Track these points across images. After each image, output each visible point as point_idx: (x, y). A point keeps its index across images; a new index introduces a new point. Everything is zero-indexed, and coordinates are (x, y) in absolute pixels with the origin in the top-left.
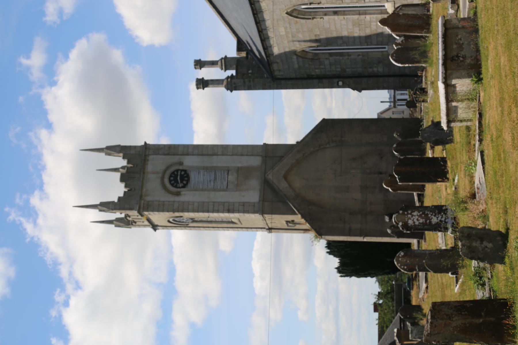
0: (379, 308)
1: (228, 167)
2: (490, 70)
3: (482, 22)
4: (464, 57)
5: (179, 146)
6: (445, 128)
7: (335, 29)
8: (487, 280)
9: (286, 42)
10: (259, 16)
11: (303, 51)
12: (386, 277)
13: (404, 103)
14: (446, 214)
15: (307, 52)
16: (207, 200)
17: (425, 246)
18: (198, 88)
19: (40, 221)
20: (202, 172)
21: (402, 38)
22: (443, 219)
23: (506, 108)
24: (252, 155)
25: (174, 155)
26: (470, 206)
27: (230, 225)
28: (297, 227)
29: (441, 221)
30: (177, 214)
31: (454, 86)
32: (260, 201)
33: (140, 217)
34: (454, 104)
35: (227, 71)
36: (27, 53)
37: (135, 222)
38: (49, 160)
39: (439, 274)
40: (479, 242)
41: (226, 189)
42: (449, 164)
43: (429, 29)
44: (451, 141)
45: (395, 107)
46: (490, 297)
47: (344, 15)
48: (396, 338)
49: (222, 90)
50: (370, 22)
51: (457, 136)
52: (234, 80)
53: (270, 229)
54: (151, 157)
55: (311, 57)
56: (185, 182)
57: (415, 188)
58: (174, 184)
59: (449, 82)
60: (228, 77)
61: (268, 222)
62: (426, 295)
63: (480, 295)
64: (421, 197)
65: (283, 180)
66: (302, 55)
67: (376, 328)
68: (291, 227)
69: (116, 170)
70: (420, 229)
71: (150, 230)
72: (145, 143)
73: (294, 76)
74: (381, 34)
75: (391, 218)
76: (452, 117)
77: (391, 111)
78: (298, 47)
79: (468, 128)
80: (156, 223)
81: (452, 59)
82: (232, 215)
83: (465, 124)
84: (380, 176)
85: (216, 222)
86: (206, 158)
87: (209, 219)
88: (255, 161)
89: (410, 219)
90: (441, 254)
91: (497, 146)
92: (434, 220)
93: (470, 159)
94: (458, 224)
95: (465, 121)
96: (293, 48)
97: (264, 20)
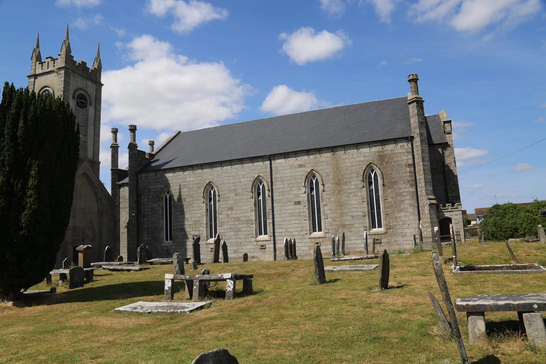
1: (87, 136)
7: (191, 210)
24: (93, 153)
25: (95, 101)
55: (161, 196)
58: (79, 96)
65: (83, 172)
72: (103, 85)
84: (82, 239)
86: (93, 121)
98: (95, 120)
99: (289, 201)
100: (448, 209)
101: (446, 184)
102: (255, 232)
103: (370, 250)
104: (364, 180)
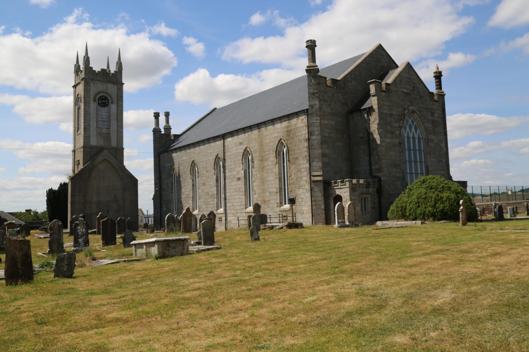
0: (28, 213)
1: (110, 128)
2: (162, 263)
3: (186, 257)
4: (169, 250)
5: (122, 102)
6: (132, 243)
8: (45, 269)
9: (179, 160)
10: (192, 146)
11: (174, 169)
12: (47, 216)
13: (147, 222)
14: (84, 246)
15: (173, 171)
16: (91, 116)
17: (65, 236)
18: (154, 113)
19: (76, 26)
20: (108, 114)
21: (180, 219)
22: (81, 245)
23: (142, 272)
24: (117, 142)
26: (88, 258)
27: (77, 129)
28: (76, 167)
29: (80, 244)
30: (83, 99)
31: (154, 246)
32: (91, 146)
33: (81, 78)
34: (145, 247)
35: (163, 129)
36: (168, 25)
37: (77, 76)
38: (110, 33)
39: (48, 244)
40: (67, 263)
41: (97, 127)
42: (112, 246)
43: (184, 232)
44: (125, 247)
45: (145, 217)
46: (35, 271)
47: (192, 190)
48: (9, 222)
49: (153, 126)
50: (189, 203)
51: (127, 250)
52: (158, 133)
53: (74, 151)
54: (116, 87)
56: (101, 104)
57: (99, 229)
59: (156, 243)
60: (160, 130)
61: (79, 150)
62: (36, 238)
63: (36, 266)
64: (94, 233)
66: (172, 168)
67: (16, 211)
68: (76, 163)
69: (108, 67)
70: (75, 233)
71: (73, 84)
72: (124, 84)
73: (161, 164)
74: (182, 209)
75: (81, 217)
76: (138, 246)
77: (143, 216)
78: (176, 166)
79: (132, 255)
80: (77, 88)
81: (168, 244)
82: (82, 130)
83: (134, 253)
85: (78, 121)
87: (80, 117)
88: (114, 143)
89: (81, 227)
90: (61, 245)
91: (121, 270)
92: (80, 240)
93: (115, 256)
94: (78, 252)
95: (136, 253)
96: (175, 164)
97: (190, 149)
98: (117, 115)
99: (234, 177)
100: (338, 186)
101: (370, 155)
102: (216, 206)
103: (232, 225)
104: (277, 156)
